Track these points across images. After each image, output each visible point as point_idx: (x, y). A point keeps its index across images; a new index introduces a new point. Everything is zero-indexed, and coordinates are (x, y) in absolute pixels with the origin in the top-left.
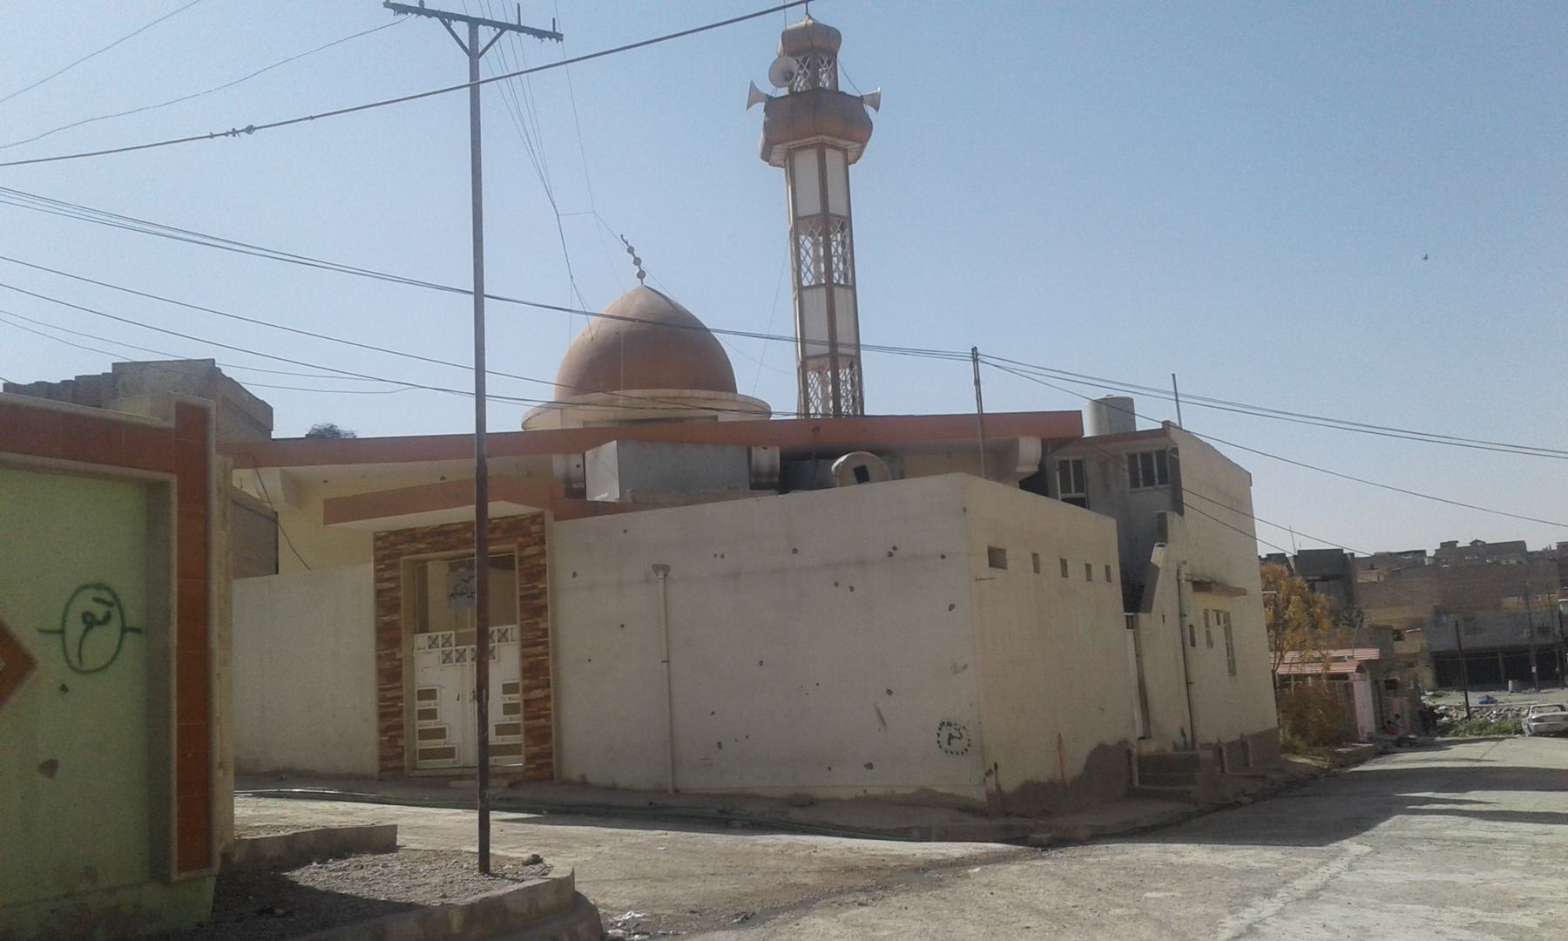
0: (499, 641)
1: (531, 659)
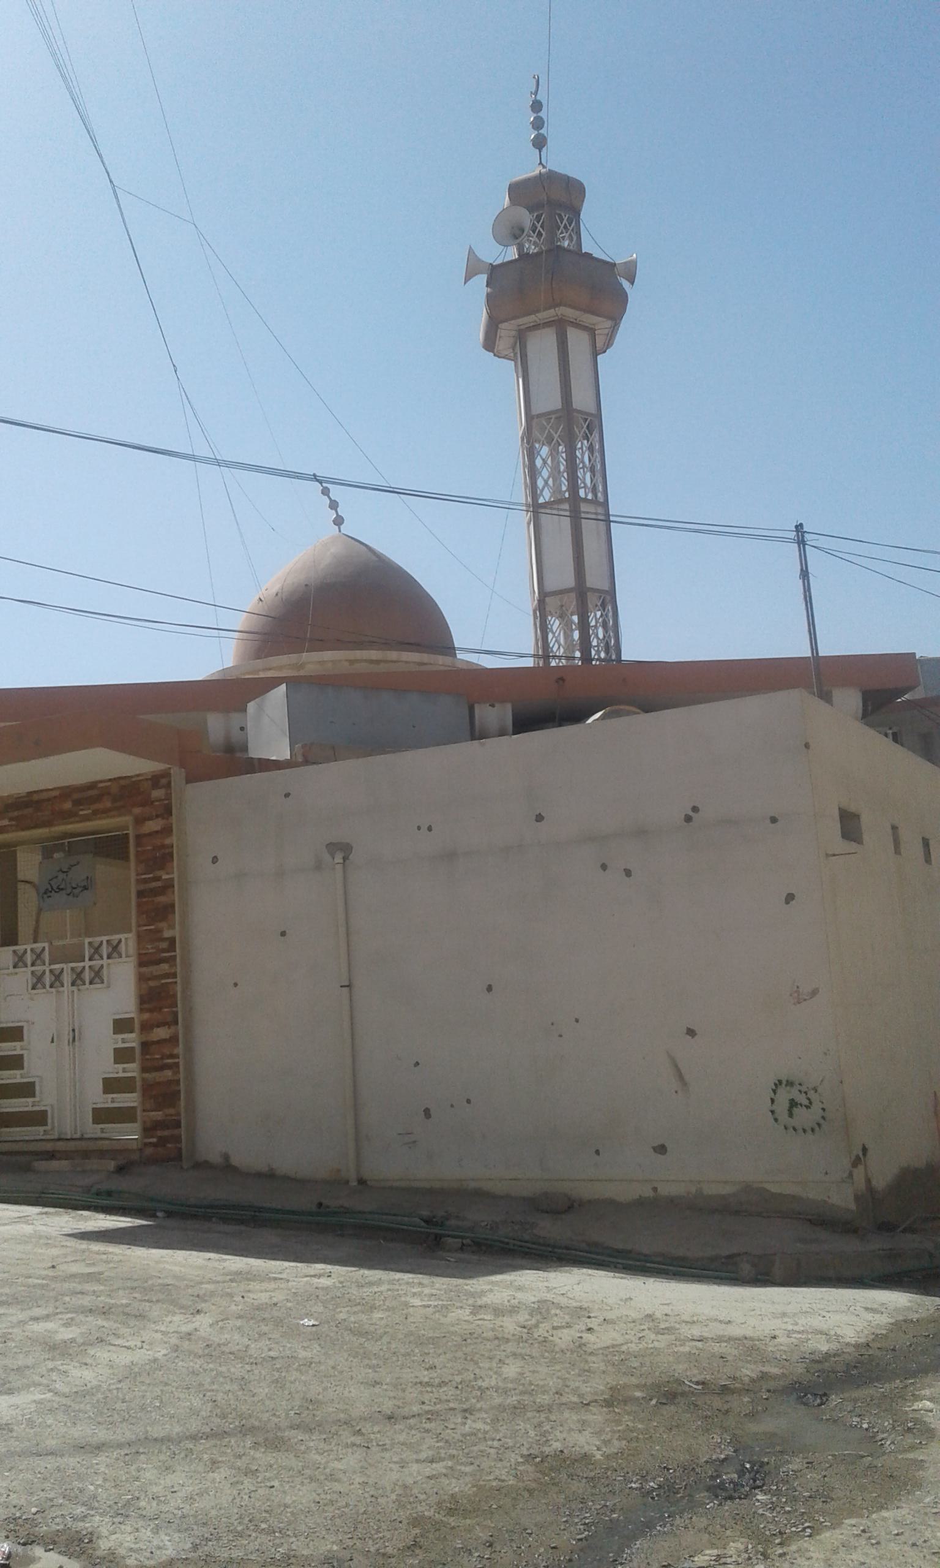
0: (109, 957)
1: (152, 983)
